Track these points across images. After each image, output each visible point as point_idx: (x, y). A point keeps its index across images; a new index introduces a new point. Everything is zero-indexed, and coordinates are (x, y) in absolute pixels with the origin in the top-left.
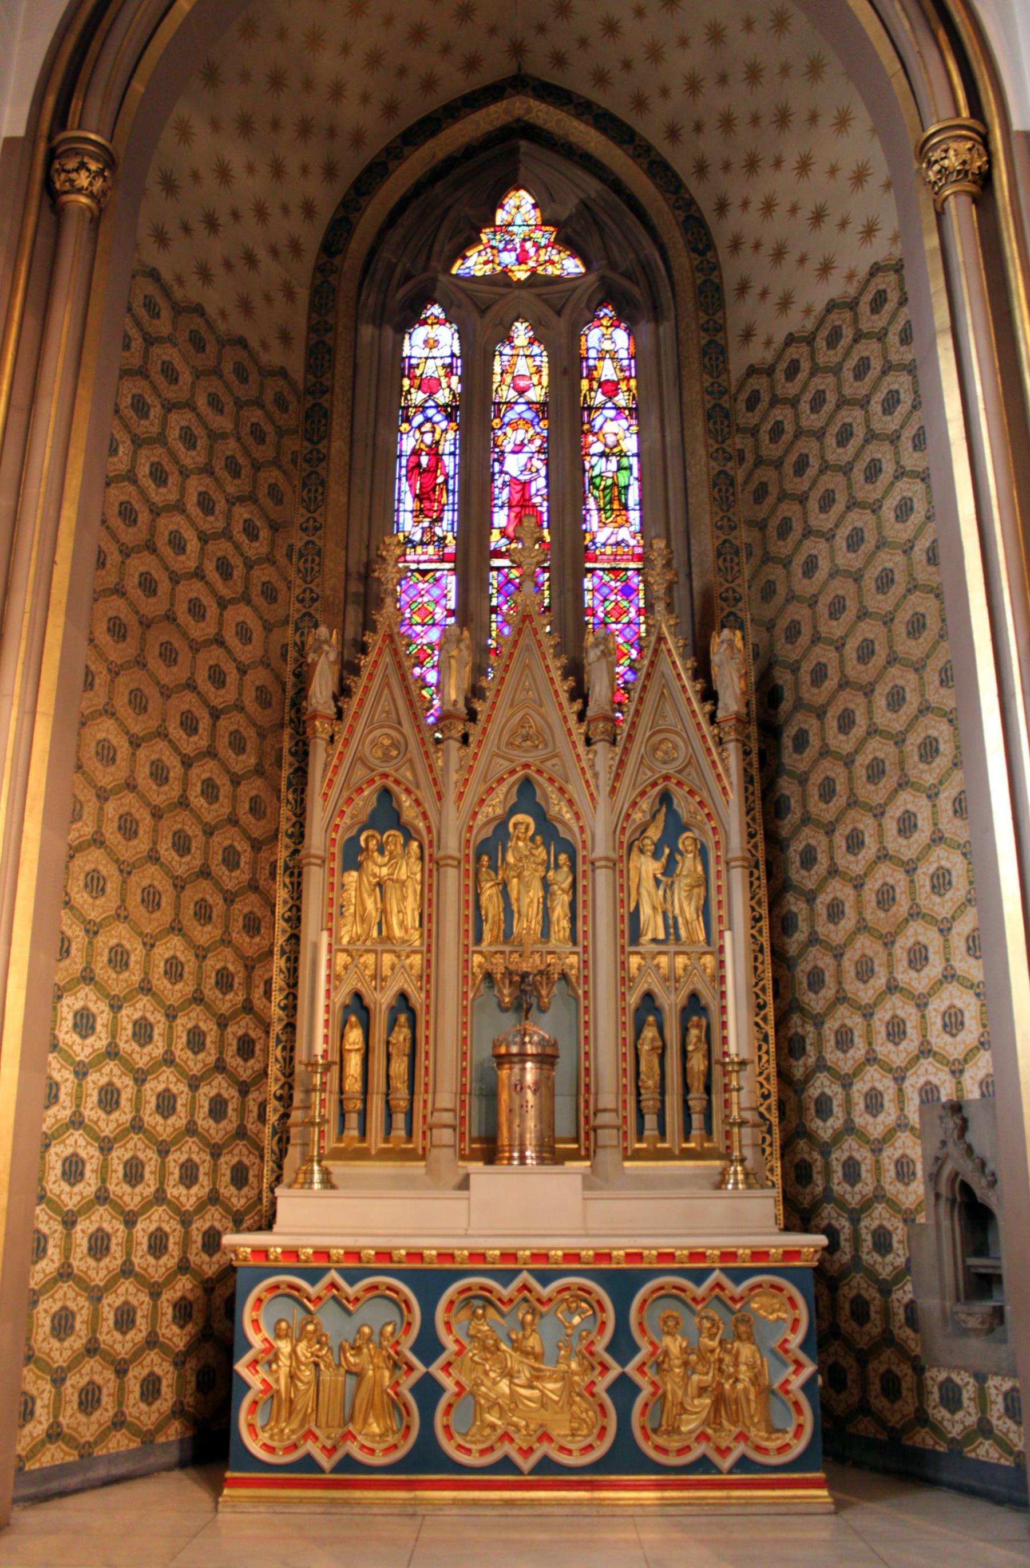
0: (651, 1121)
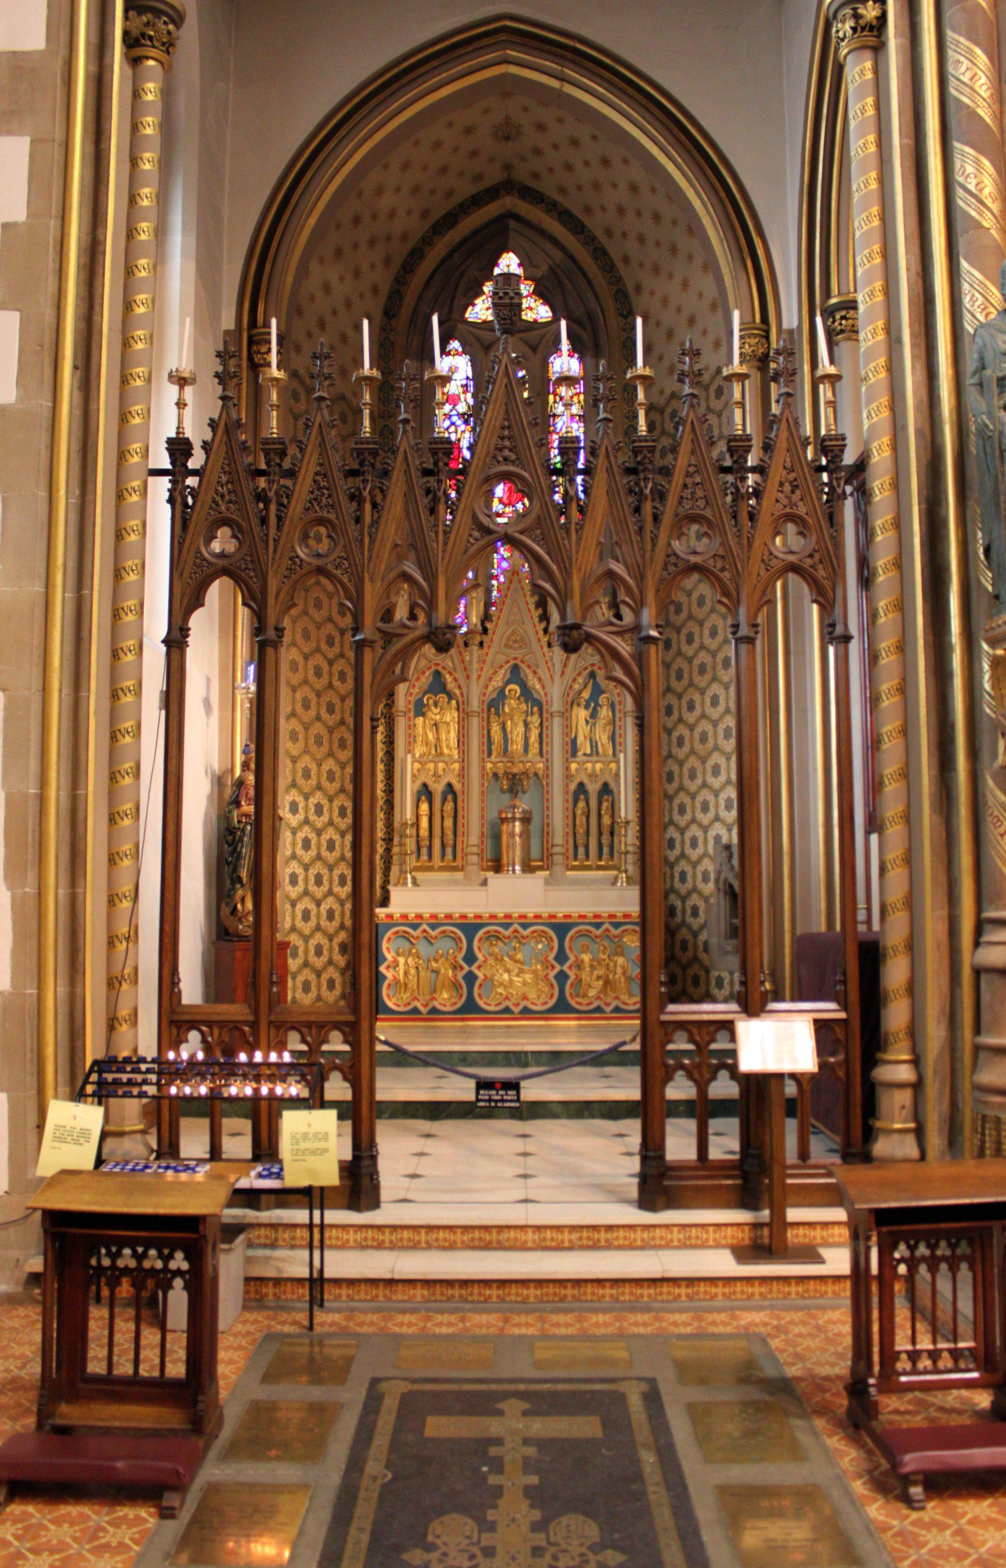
0: (581, 850)
